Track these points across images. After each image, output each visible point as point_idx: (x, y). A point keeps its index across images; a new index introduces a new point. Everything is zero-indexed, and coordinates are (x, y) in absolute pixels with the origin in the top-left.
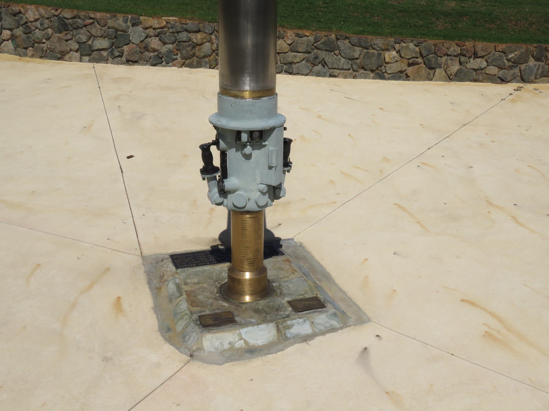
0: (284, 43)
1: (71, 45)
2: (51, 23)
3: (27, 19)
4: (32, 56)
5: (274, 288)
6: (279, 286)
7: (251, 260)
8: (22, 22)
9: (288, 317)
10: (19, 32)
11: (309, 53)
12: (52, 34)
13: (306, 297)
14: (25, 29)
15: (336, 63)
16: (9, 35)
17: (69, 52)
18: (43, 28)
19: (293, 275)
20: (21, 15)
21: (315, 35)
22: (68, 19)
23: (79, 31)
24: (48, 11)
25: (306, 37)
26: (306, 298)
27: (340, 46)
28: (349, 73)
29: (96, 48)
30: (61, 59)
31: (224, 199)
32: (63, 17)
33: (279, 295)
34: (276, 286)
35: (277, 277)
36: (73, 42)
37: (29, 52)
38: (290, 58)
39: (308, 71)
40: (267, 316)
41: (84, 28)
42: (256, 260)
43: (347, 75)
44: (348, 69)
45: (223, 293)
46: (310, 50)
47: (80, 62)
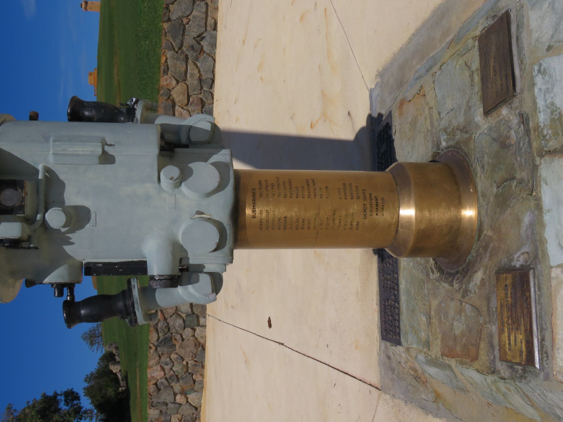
0: (175, 89)
1: (187, 335)
2: (164, 355)
3: (162, 377)
4: (202, 375)
5: (451, 146)
6: (447, 132)
7: (368, 206)
8: (166, 383)
9: (528, 119)
10: (177, 387)
11: (187, 58)
12: (177, 354)
13: (479, 68)
14: (173, 380)
15: (199, 21)
16: (181, 396)
17: (196, 339)
18: (171, 363)
19: (428, 97)
20: (158, 383)
21: (165, 49)
22: (159, 337)
23: (172, 326)
24: (151, 356)
25: (168, 61)
26: (481, 66)
27: (178, 16)
28: (212, 4)
29: (190, 310)
30: (204, 347)
31: (205, 270)
32: (157, 342)
33: (467, 136)
34: (447, 141)
35: (428, 134)
36: (184, 333)
37: (198, 379)
38: (194, 82)
39: (210, 59)
40: (518, 176)
41: (168, 320)
42: (370, 194)
43: (213, 7)
44: (206, 5)
45: (453, 271)
46: (183, 56)
47: (206, 327)
